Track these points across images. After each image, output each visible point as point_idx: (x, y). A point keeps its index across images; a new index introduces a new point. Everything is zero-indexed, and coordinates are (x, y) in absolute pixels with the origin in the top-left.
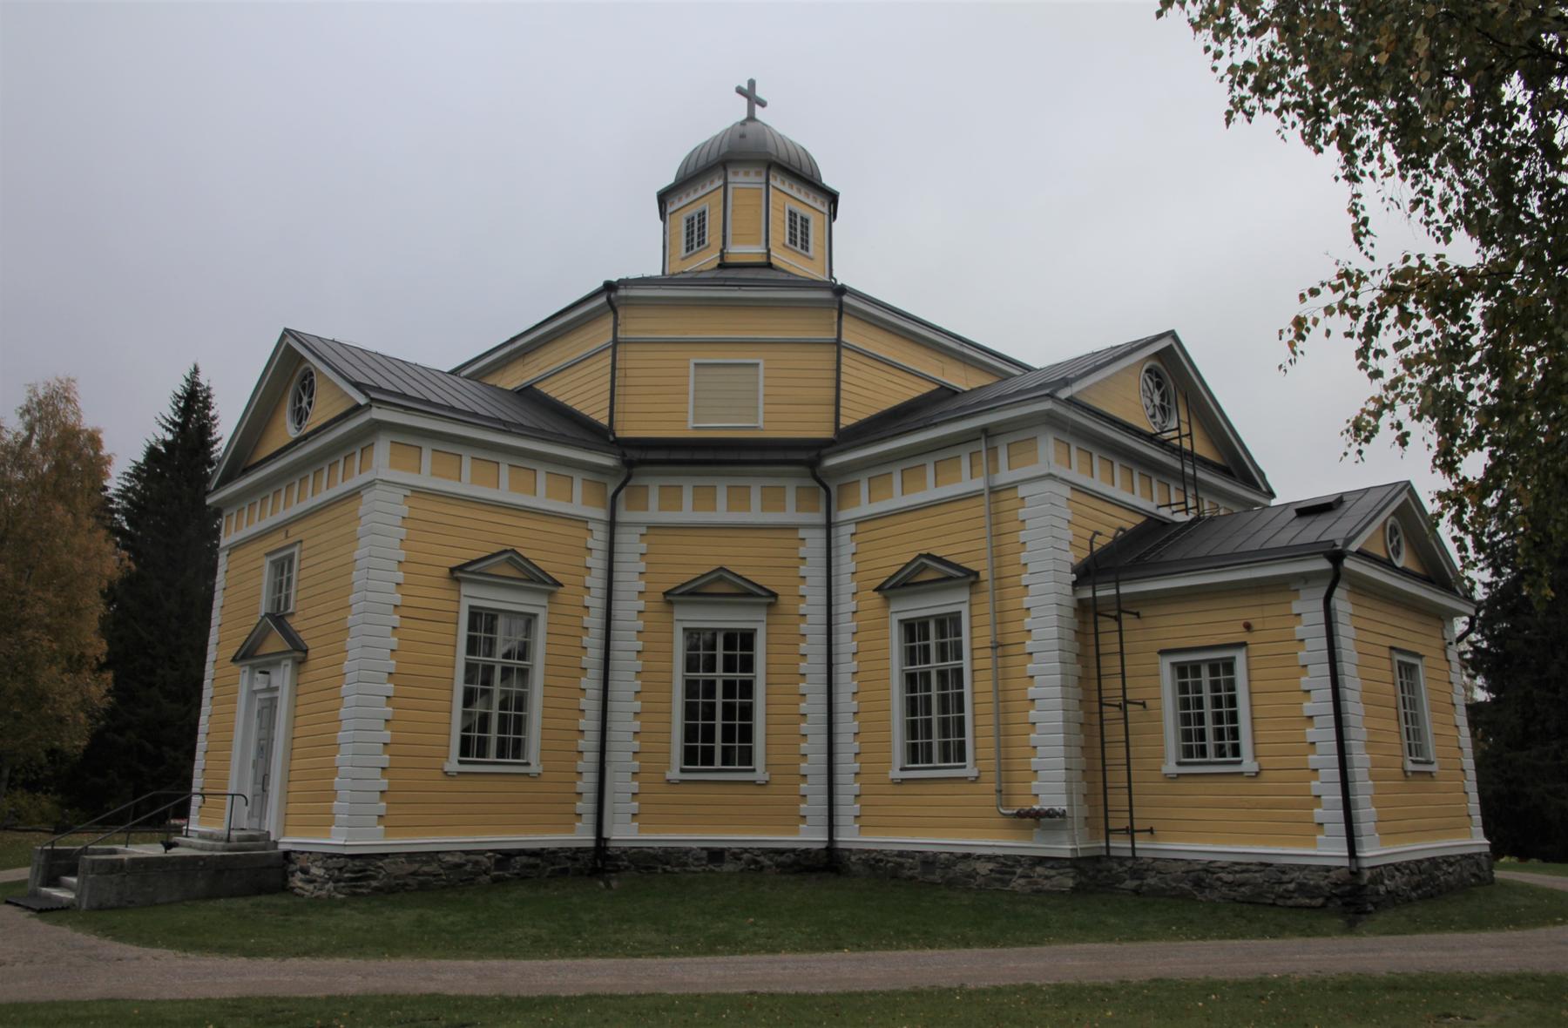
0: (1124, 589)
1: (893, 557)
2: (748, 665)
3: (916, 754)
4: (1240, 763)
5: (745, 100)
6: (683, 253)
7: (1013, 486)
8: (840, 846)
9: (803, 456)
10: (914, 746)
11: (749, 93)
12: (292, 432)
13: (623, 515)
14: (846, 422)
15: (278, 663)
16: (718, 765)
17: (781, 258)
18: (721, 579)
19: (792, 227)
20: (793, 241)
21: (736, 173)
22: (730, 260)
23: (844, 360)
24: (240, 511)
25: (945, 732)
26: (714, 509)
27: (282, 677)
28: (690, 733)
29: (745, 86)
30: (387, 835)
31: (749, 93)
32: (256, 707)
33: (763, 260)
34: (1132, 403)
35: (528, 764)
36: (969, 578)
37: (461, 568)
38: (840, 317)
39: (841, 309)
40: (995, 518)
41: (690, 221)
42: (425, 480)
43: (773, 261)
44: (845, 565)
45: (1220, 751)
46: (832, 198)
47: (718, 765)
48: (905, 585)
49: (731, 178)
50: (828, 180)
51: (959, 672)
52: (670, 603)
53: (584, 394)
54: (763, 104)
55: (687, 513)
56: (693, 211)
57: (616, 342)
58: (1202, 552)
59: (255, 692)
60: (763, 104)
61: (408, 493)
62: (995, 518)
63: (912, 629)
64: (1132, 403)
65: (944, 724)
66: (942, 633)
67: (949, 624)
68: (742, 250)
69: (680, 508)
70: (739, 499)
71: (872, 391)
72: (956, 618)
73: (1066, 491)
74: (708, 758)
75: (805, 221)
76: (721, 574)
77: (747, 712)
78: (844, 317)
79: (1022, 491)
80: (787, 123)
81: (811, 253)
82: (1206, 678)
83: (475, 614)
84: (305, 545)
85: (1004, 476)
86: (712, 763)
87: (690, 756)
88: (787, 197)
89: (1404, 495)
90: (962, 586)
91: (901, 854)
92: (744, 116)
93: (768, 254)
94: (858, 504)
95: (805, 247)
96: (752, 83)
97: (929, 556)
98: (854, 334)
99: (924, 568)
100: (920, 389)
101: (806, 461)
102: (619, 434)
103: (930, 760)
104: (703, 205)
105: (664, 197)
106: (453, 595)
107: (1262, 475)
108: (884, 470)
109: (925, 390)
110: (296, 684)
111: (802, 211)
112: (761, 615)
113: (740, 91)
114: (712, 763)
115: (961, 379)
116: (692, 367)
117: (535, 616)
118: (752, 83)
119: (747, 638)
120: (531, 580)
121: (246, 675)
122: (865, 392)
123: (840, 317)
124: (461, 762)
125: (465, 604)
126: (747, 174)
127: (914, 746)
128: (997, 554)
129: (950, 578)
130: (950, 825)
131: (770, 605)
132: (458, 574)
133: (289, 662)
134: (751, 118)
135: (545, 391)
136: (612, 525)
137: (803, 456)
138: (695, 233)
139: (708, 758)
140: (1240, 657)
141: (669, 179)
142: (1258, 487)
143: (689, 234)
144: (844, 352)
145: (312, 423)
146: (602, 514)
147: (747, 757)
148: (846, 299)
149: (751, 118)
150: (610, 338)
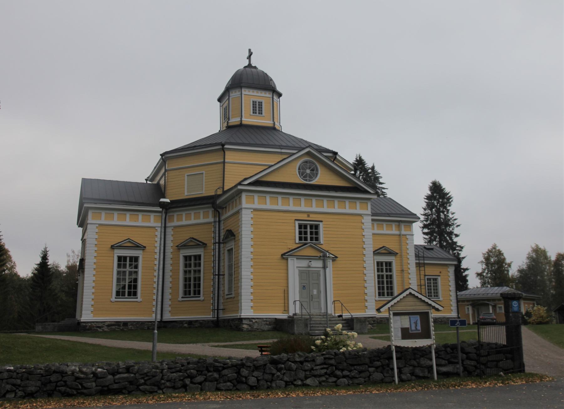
0: (425, 262)
1: (184, 236)
3: (187, 293)
4: (199, 297)
7: (405, 235)
13: (168, 224)
16: (126, 296)
24: (229, 204)
25: (195, 287)
30: (94, 317)
33: (272, 125)
36: (143, 248)
40: (400, 242)
42: (256, 206)
44: (169, 238)
45: (129, 294)
46: (280, 95)
47: (126, 296)
48: (185, 246)
50: (279, 89)
62: (400, 242)
63: (187, 258)
65: (195, 285)
66: (195, 260)
67: (389, 264)
69: (200, 219)
70: (188, 217)
72: (200, 256)
82: (432, 281)
85: (403, 232)
90: (201, 247)
91: (381, 318)
93: (274, 124)
94: (173, 221)
103: (190, 294)
116: (186, 177)
119: (136, 259)
122: (386, 207)
128: (401, 249)
129: (199, 245)
131: (143, 250)
132: (113, 247)
139: (123, 294)
140: (439, 278)
147: (135, 294)
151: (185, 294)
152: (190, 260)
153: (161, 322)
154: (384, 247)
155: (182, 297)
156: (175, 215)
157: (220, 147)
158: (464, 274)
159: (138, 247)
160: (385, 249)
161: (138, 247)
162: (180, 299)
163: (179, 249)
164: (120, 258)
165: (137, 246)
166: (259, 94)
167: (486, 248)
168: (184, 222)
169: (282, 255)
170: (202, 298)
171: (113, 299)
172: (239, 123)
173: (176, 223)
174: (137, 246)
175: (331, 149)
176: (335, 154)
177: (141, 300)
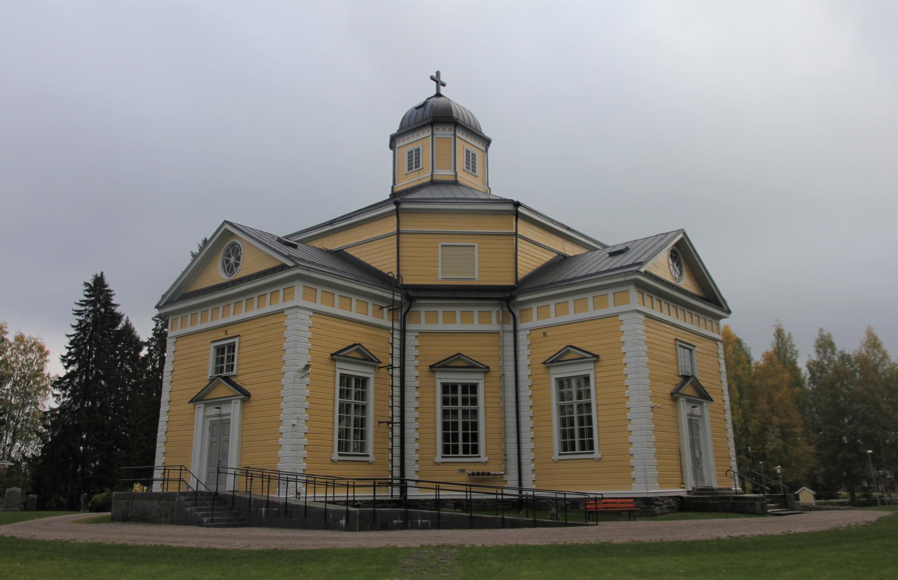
2: (474, 401)
3: (568, 447)
5: (435, 83)
6: (406, 171)
8: (408, 498)
9: (500, 295)
10: (362, 427)
11: (436, 79)
12: (224, 278)
13: (409, 327)
14: (520, 277)
15: (230, 402)
16: (461, 454)
17: (464, 177)
18: (459, 359)
19: (468, 160)
20: (468, 168)
21: (437, 129)
22: (435, 178)
23: (519, 244)
26: (455, 323)
27: (234, 410)
28: (446, 438)
29: (435, 75)
31: (436, 79)
32: (208, 424)
33: (453, 179)
34: (661, 266)
35: (368, 456)
36: (486, 370)
37: (337, 354)
38: (517, 220)
39: (517, 215)
41: (410, 153)
43: (459, 179)
45: (466, 451)
46: (487, 142)
47: (461, 454)
49: (435, 132)
50: (486, 132)
51: (589, 405)
52: (334, 360)
53: (382, 259)
54: (444, 85)
55: (441, 326)
56: (413, 147)
57: (398, 233)
58: (549, 282)
59: (208, 417)
60: (444, 85)
61: (311, 314)
64: (661, 266)
65: (582, 432)
68: (443, 173)
71: (531, 259)
72: (587, 379)
73: (642, 317)
74: (455, 450)
75: (474, 155)
76: (458, 356)
77: (475, 426)
78: (519, 220)
79: (621, 317)
80: (457, 96)
81: (477, 174)
83: (342, 376)
84: (244, 338)
86: (457, 453)
87: (446, 450)
88: (464, 143)
89: (681, 236)
92: (434, 92)
93: (456, 175)
95: (474, 171)
96: (438, 73)
97: (571, 346)
98: (524, 229)
99: (568, 351)
100: (548, 257)
101: (505, 298)
102: (405, 282)
103: (573, 449)
104: (419, 145)
105: (394, 139)
106: (332, 368)
107: (725, 301)
108: (545, 303)
109: (551, 258)
110: (243, 413)
111: (472, 150)
112: (481, 376)
113: (432, 78)
114: (457, 453)
115: (570, 250)
117: (368, 378)
118: (438, 73)
119: (474, 388)
120: (366, 360)
121: (202, 410)
123: (517, 220)
124: (340, 455)
125: (338, 372)
126: (444, 130)
127: (362, 427)
130: (577, 479)
131: (486, 372)
132: (336, 356)
133: (239, 401)
134: (438, 95)
135: (351, 253)
136: (403, 332)
137: (500, 295)
138: (414, 161)
139: (455, 450)
141: (395, 129)
142: (721, 306)
143: (410, 161)
144: (519, 240)
145: (240, 273)
146: (397, 326)
147: (475, 450)
148: (520, 209)
149: (438, 95)
150: (395, 230)
151: (565, 449)
152: (570, 386)
153: (179, 492)
154: (355, 345)
155: (560, 454)
156: (423, 311)
157: (510, 207)
158: (808, 386)
159: (474, 367)
160: (357, 350)
161: (474, 367)
162: (556, 457)
163: (548, 368)
164: (445, 388)
165: (473, 367)
166: (411, 140)
167: (816, 336)
168: (441, 326)
169: (431, 367)
170: (597, 454)
171: (439, 458)
172: (429, 179)
173: (424, 326)
174: (473, 367)
175: (509, 198)
176: (517, 204)
177: (486, 459)
